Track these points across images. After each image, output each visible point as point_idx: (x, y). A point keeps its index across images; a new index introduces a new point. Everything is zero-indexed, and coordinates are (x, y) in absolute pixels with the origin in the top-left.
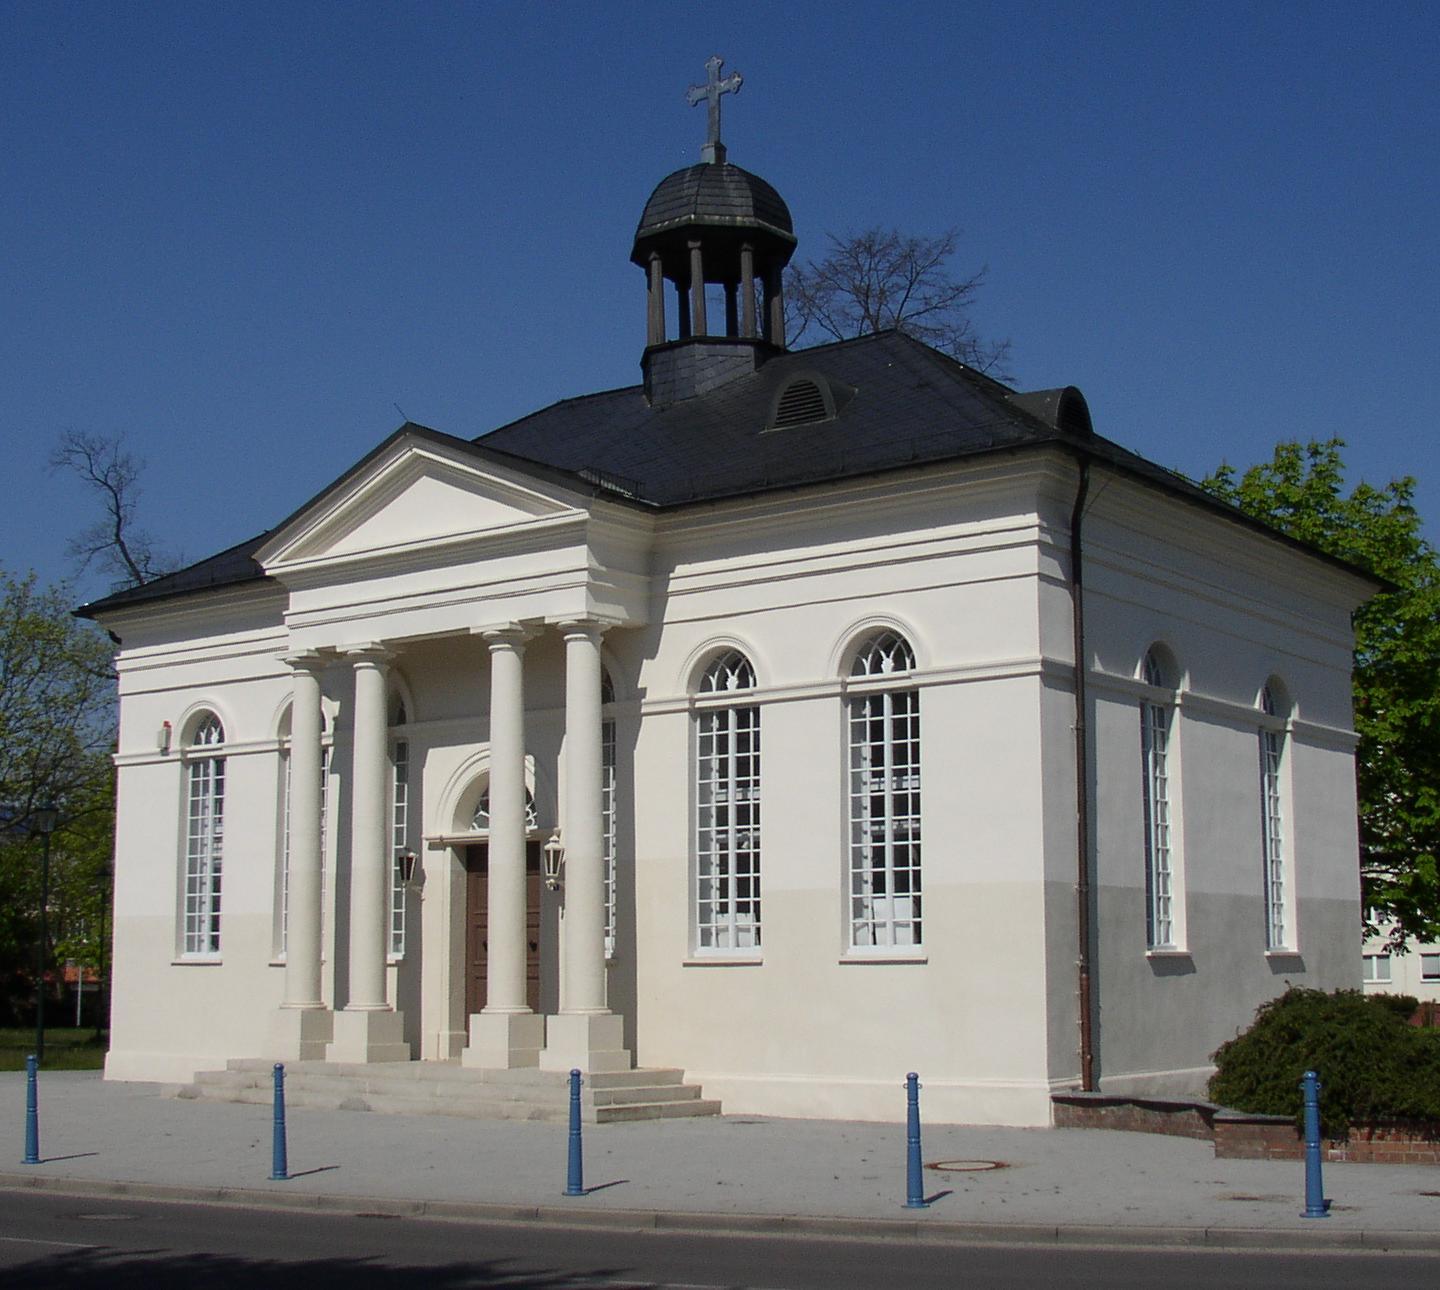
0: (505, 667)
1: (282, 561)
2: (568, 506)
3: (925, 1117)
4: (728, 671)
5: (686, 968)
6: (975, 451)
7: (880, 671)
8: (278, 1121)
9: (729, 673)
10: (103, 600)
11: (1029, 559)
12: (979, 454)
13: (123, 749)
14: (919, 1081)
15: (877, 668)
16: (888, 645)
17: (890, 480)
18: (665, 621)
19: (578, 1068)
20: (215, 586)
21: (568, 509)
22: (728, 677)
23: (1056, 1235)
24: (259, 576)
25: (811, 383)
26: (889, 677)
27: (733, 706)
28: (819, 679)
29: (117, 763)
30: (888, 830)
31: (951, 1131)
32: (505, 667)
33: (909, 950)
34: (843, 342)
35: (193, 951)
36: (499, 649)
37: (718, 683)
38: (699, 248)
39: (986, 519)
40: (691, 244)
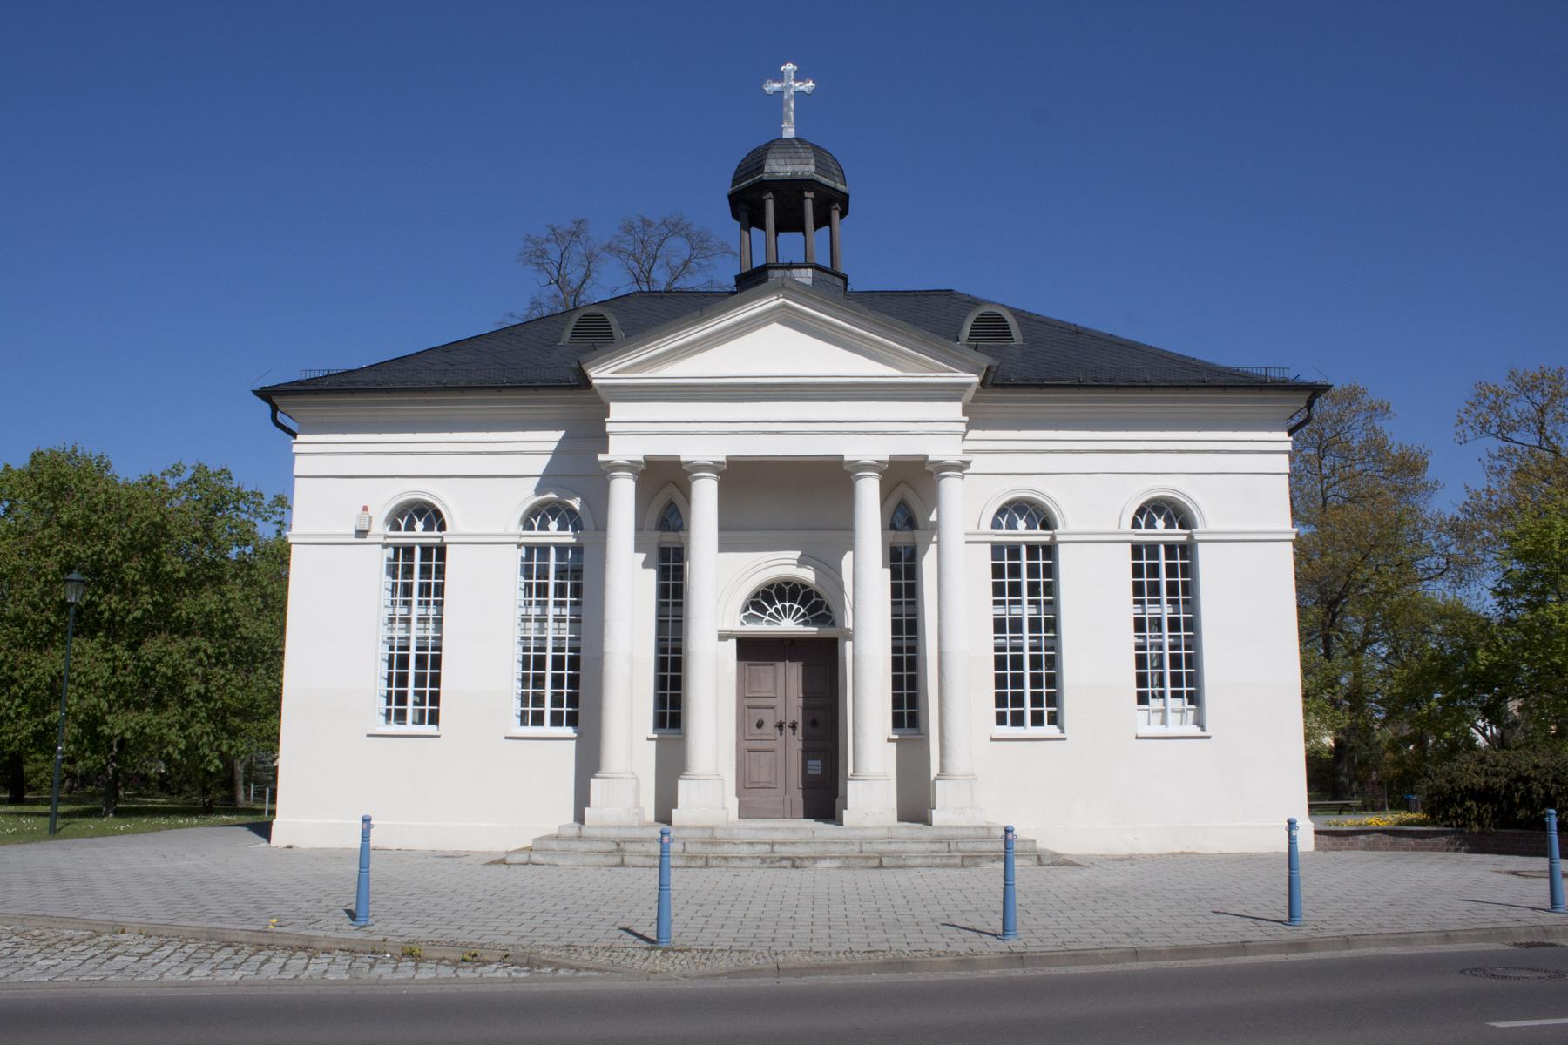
0: (869, 492)
1: (613, 373)
2: (955, 370)
3: (375, 841)
4: (399, 520)
5: (507, 740)
6: (1115, 384)
7: (413, 530)
8: (665, 888)
9: (550, 519)
10: (284, 384)
11: (1283, 463)
12: (1092, 386)
13: (295, 530)
14: (372, 822)
15: (410, 527)
16: (1035, 512)
17: (1012, 394)
18: (538, 479)
19: (1014, 827)
20: (317, 392)
21: (613, 373)
22: (1155, 520)
23: (1348, 942)
24: (585, 383)
25: (999, 315)
26: (420, 533)
27: (1163, 542)
28: (501, 531)
29: (290, 540)
30: (1026, 643)
31: (403, 855)
32: (869, 492)
33: (1196, 731)
34: (642, 292)
35: (527, 725)
36: (871, 476)
37: (1146, 524)
38: (812, 199)
39: (976, 429)
40: (807, 194)
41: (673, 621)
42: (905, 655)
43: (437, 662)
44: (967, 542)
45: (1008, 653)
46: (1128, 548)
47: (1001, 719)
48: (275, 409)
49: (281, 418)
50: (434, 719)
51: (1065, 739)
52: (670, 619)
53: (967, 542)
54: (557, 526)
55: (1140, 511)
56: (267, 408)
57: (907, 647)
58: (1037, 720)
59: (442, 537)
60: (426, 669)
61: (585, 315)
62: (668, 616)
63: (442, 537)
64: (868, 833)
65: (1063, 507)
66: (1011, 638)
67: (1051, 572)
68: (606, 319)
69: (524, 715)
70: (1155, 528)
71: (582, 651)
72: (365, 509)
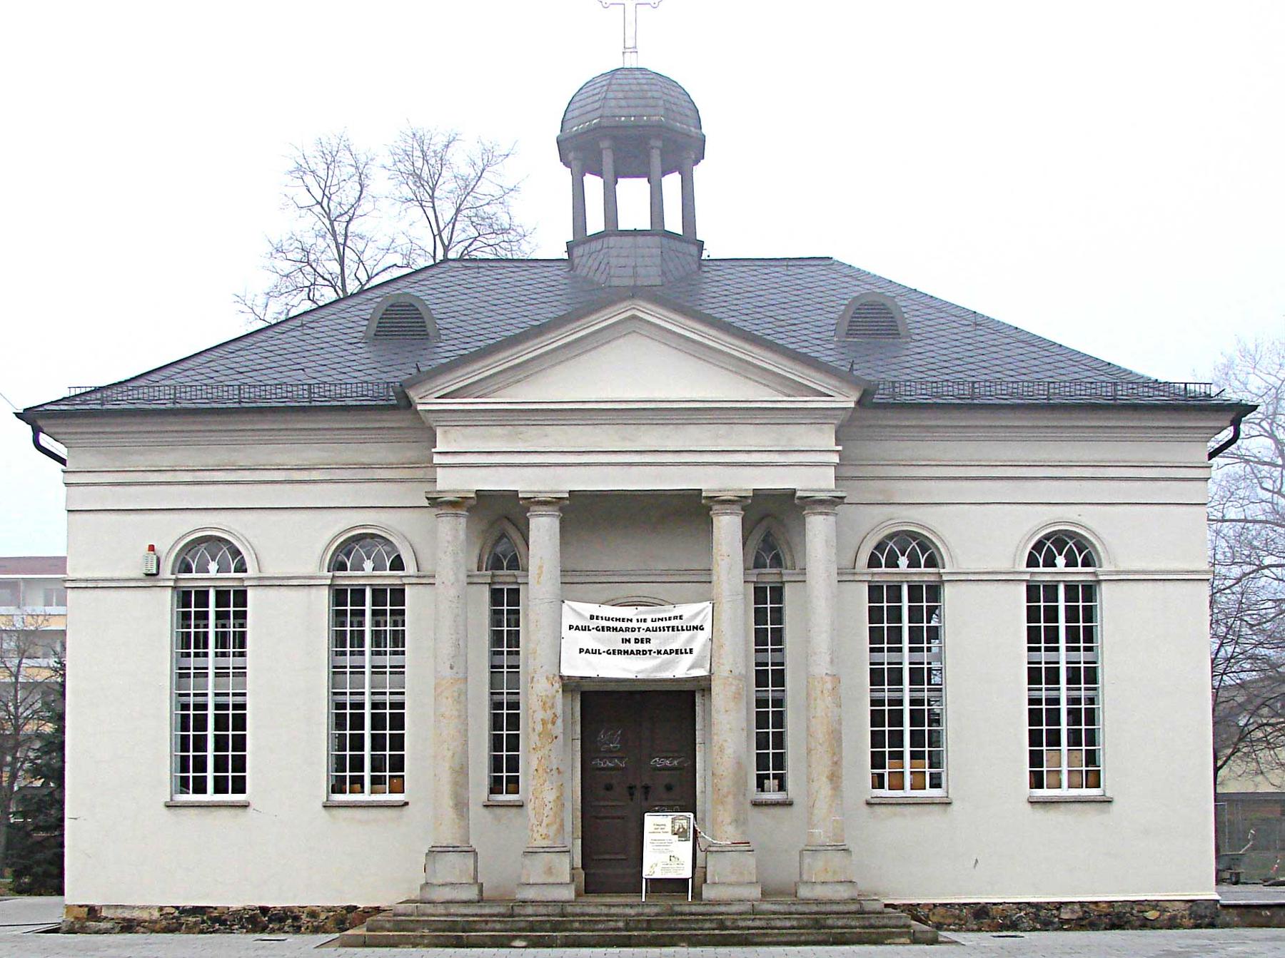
5: (757, 810)
22: (1055, 557)
25: (883, 305)
41: (351, 673)
42: (191, 712)
43: (240, 722)
44: (839, 581)
45: (231, 712)
46: (1023, 589)
47: (878, 782)
48: (36, 431)
49: (45, 440)
50: (240, 787)
51: (245, 806)
52: (505, 670)
53: (468, 584)
54: (1064, 561)
55: (1038, 546)
56: (27, 430)
57: (351, 704)
58: (220, 787)
59: (1094, 574)
60: (1042, 725)
61: (392, 306)
62: (507, 672)
63: (781, 574)
64: (136, 914)
65: (1103, 535)
66: (1086, 689)
67: (1092, 618)
68: (417, 310)
69: (184, 782)
70: (1055, 566)
71: (248, 706)
72: (152, 548)
